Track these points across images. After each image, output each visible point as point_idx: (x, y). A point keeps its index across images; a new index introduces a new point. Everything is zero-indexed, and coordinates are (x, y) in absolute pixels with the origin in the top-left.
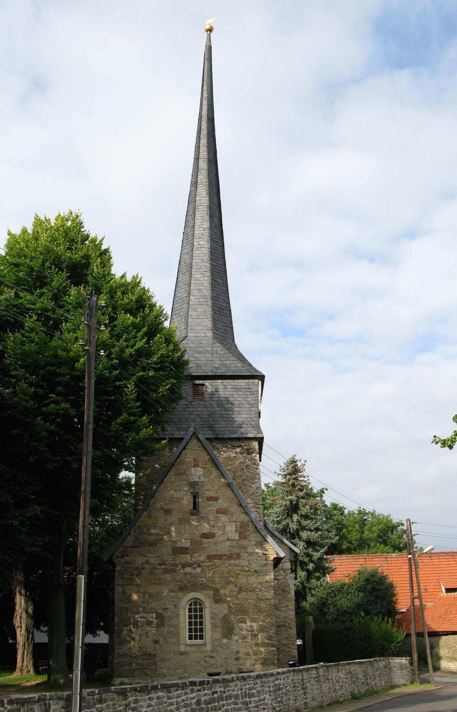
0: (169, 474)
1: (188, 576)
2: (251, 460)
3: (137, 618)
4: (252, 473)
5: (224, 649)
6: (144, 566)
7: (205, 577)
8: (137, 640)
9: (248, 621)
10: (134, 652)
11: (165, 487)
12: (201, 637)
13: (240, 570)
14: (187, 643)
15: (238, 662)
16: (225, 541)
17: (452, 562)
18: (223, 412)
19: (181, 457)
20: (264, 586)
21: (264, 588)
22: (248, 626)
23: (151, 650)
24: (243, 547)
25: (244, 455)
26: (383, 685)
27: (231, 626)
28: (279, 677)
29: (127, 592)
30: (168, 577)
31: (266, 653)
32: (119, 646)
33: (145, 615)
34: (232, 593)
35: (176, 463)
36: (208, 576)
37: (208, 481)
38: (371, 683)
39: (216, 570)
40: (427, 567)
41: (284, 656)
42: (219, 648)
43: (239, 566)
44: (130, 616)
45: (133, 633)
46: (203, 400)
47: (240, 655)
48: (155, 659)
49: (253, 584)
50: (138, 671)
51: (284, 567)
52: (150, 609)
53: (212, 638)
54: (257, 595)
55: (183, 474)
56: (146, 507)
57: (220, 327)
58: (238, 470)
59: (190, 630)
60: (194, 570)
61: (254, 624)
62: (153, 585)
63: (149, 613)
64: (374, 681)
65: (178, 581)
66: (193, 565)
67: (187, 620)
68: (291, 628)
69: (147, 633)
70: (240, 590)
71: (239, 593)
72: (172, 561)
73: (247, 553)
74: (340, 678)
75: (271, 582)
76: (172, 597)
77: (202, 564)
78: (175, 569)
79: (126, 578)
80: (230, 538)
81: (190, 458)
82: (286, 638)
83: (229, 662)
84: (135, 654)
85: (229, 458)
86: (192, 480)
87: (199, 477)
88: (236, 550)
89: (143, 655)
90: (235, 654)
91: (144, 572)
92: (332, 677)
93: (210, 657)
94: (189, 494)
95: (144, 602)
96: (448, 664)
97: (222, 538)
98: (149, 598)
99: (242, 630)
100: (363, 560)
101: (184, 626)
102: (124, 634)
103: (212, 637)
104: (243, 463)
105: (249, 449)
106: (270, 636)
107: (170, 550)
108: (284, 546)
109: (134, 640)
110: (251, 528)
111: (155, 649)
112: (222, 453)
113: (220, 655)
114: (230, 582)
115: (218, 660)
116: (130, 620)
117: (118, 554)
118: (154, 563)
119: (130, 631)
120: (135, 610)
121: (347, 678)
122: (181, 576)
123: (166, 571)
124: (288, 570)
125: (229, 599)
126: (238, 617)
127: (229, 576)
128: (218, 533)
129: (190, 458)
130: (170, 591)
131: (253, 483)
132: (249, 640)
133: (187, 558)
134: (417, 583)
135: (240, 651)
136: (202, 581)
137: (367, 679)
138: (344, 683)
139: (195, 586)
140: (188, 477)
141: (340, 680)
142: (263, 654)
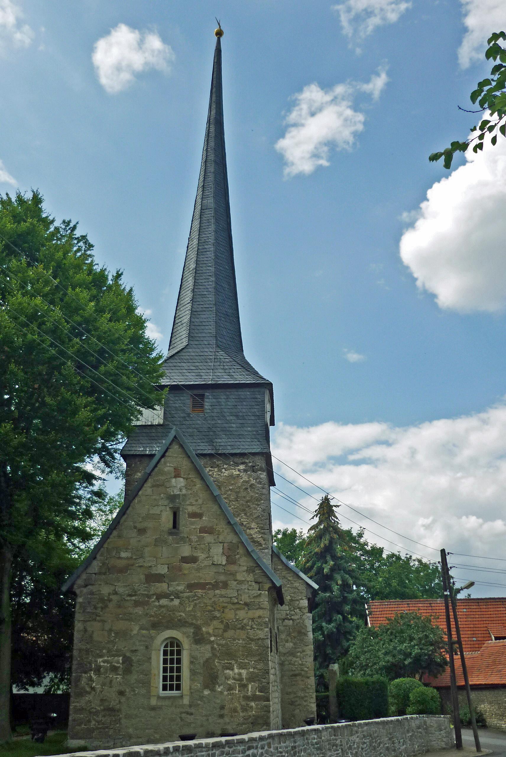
0: (145, 485)
1: (163, 609)
2: (257, 479)
3: (99, 663)
4: (257, 493)
5: (205, 703)
6: (111, 597)
7: (184, 612)
8: (98, 691)
9: (235, 667)
10: (93, 706)
11: (139, 502)
12: (178, 688)
13: (228, 603)
14: (160, 695)
15: (222, 720)
16: (210, 566)
17: (502, 609)
18: (226, 425)
19: (159, 466)
20: (256, 623)
21: (256, 625)
22: (235, 674)
23: (115, 704)
24: (231, 574)
25: (249, 473)
26: (416, 749)
27: (215, 673)
28: (254, 745)
29: (89, 629)
30: (139, 611)
31: (257, 708)
32: (76, 699)
33: (109, 658)
34: (216, 631)
35: (153, 473)
36: (187, 609)
37: (191, 494)
38: (400, 748)
39: (197, 602)
40: (474, 613)
41: (300, 711)
42: (199, 702)
43: (225, 597)
44: (91, 660)
45: (94, 682)
46: (203, 412)
47: (226, 712)
48: (119, 715)
49: (243, 620)
50: (98, 731)
51: (300, 605)
52: (117, 651)
53: (190, 689)
54: (248, 634)
55: (161, 486)
56: (117, 525)
57: (225, 335)
58: (242, 490)
59: (165, 679)
60: (170, 602)
61: (243, 671)
62: (121, 621)
63: (114, 656)
64: (403, 745)
65: (152, 616)
66: (170, 596)
67: (162, 666)
68: (308, 678)
69: (111, 681)
70: (227, 627)
71: (225, 631)
72: (145, 590)
73: (236, 580)
74: (354, 743)
75: (265, 617)
76: (144, 636)
77: (181, 595)
78: (148, 601)
79: (89, 612)
80: (215, 563)
81: (170, 466)
82: (303, 690)
83: (211, 720)
84: (95, 709)
85: (231, 476)
86: (172, 493)
87: (181, 490)
88: (222, 578)
89: (104, 710)
90: (218, 710)
91: (111, 605)
92: (341, 741)
93: (188, 713)
94: (168, 509)
95: (109, 642)
96: (498, 722)
97: (206, 563)
98: (115, 637)
99: (227, 678)
100: (406, 606)
101: (156, 673)
102: (83, 682)
103: (190, 687)
104: (247, 482)
105: (254, 466)
106: (263, 686)
107: (142, 577)
108: (300, 581)
109: (94, 691)
110: (241, 551)
111: (120, 702)
112: (223, 470)
113: (200, 710)
114: (215, 618)
115: (197, 718)
116: (91, 665)
117: (80, 582)
118: (123, 594)
119: (91, 679)
120: (98, 652)
121: (365, 743)
122: (155, 609)
123: (137, 604)
124: (305, 608)
125: (212, 639)
126: (223, 662)
127: (213, 609)
128: (202, 556)
129: (170, 466)
130: (142, 628)
131: (258, 505)
132: (237, 692)
133: (163, 587)
134: (456, 625)
135: (225, 706)
136: (180, 616)
137: (393, 743)
138: (360, 749)
139: (172, 624)
140: (168, 489)
141: (354, 745)
142: (254, 710)
